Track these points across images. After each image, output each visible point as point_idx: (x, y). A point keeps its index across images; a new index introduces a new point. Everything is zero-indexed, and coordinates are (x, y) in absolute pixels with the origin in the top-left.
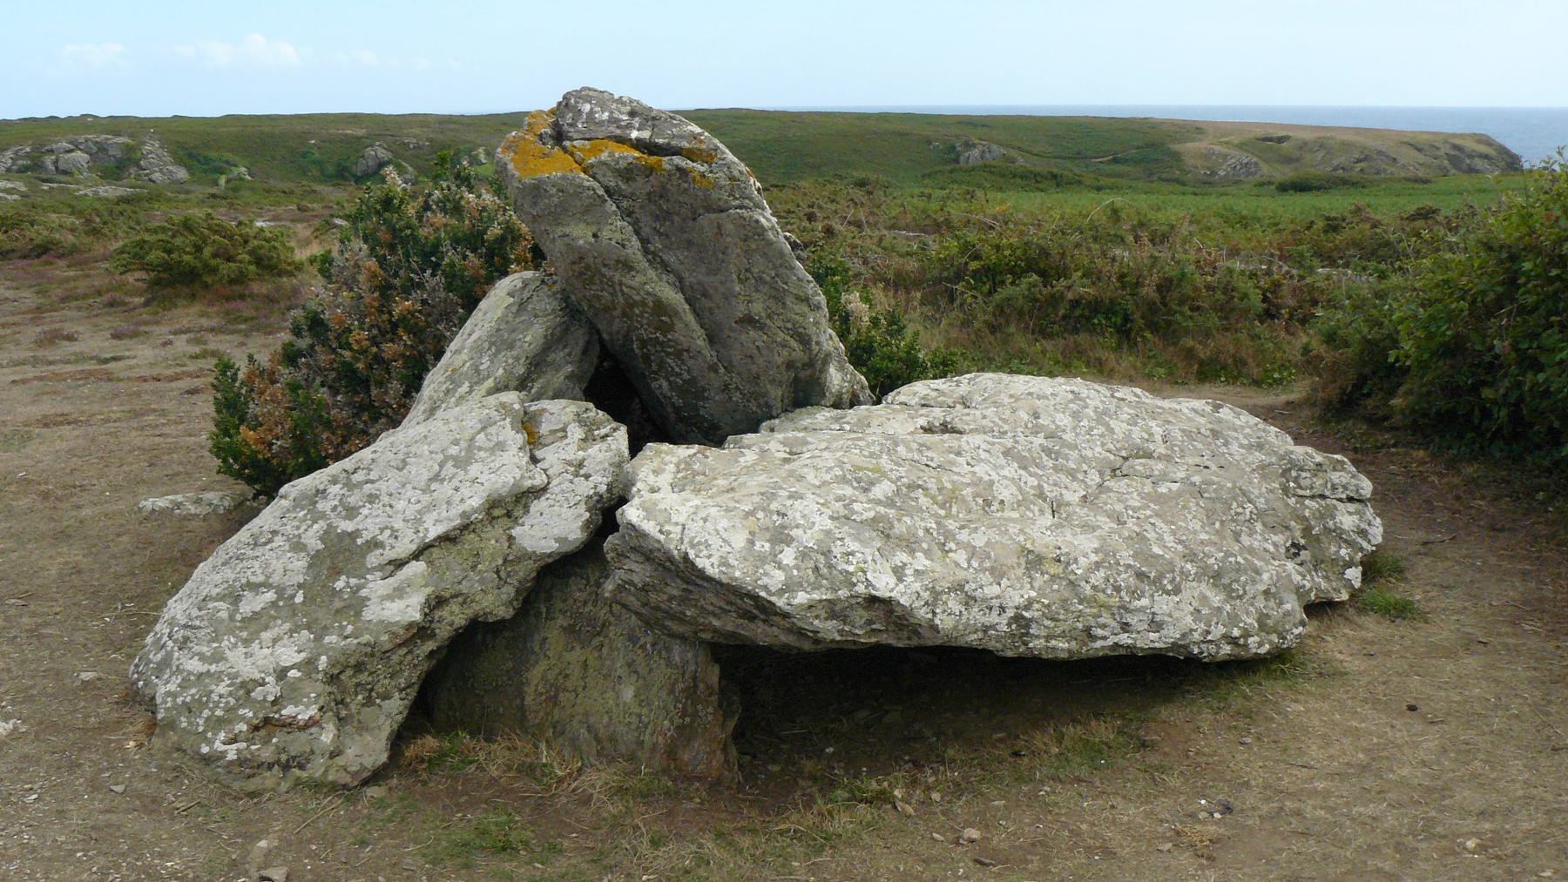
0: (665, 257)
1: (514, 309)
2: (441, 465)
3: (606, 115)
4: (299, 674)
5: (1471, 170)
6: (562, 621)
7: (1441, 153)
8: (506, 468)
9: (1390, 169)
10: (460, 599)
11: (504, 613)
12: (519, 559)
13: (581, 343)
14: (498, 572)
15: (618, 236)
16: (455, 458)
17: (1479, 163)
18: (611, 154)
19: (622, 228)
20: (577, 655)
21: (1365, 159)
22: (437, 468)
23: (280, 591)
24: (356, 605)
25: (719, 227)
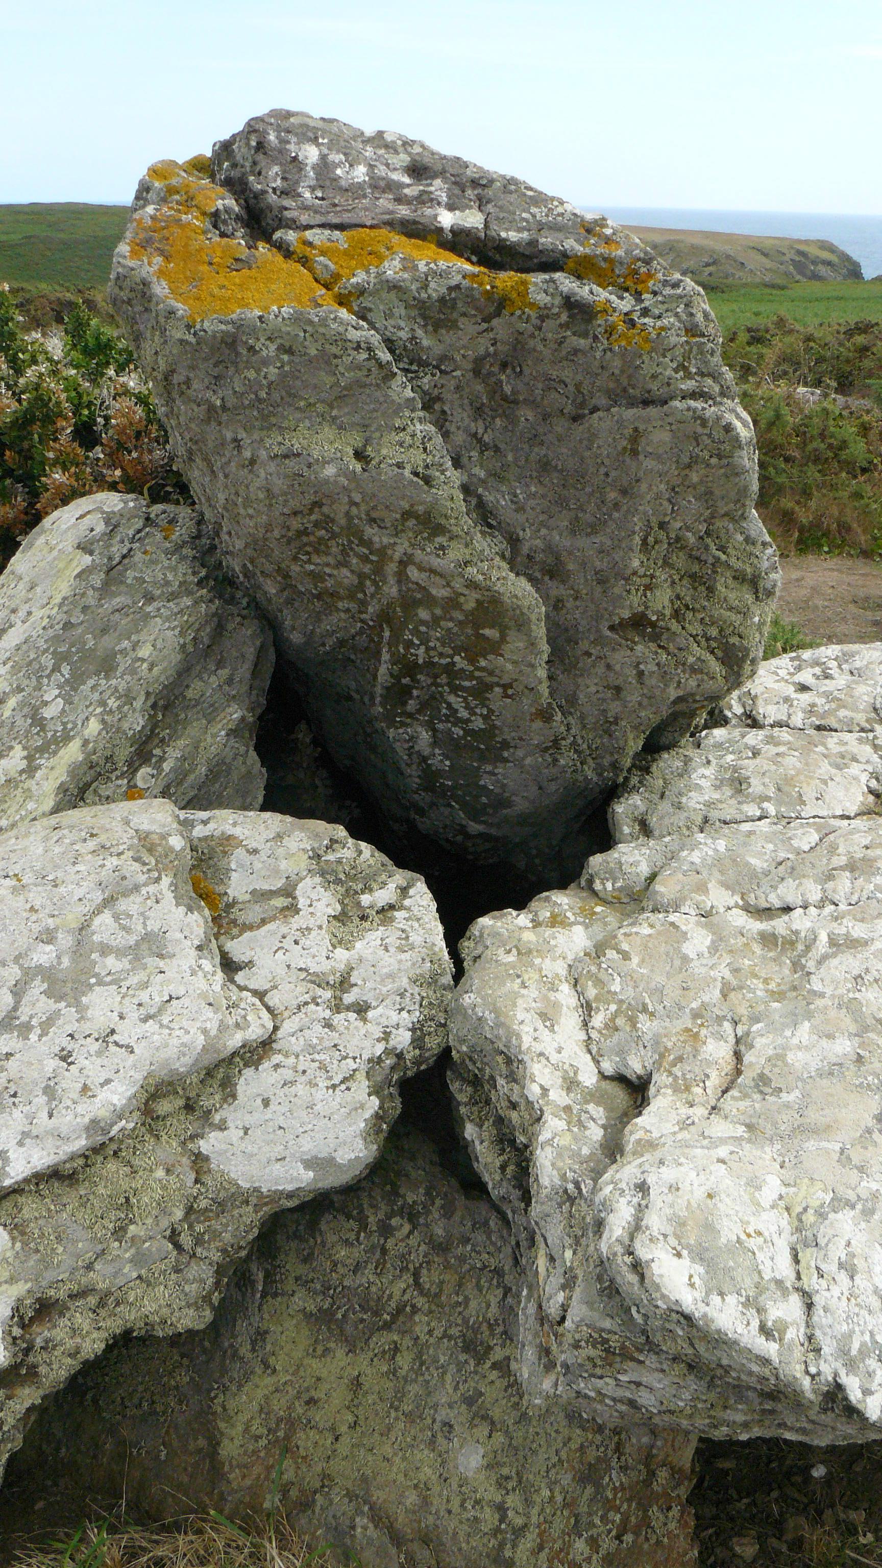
0: (489, 498)
1: (97, 580)
2: (18, 991)
3: (360, 173)
5: (815, 277)
6: (301, 1300)
7: (787, 258)
8: (176, 1010)
9: (739, 274)
10: (92, 1300)
11: (190, 1319)
12: (221, 1206)
13: (250, 652)
14: (173, 1237)
15: (417, 458)
16: (48, 974)
17: (822, 270)
18: (409, 265)
19: (427, 438)
20: (338, 1364)
21: (714, 263)
22: (9, 999)
25: (636, 436)
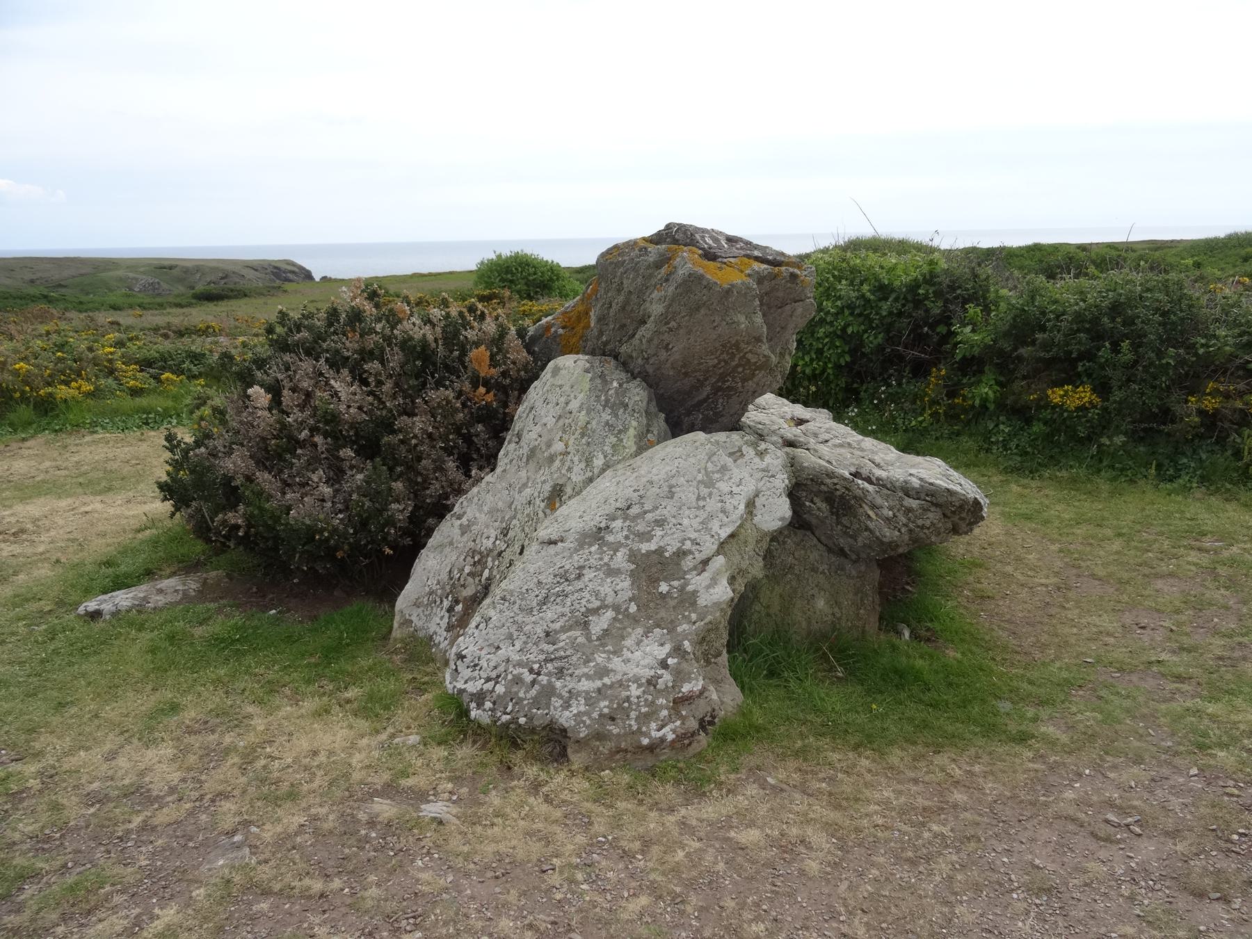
4: (676, 660)
17: (290, 276)
23: (616, 608)
24: (689, 600)
